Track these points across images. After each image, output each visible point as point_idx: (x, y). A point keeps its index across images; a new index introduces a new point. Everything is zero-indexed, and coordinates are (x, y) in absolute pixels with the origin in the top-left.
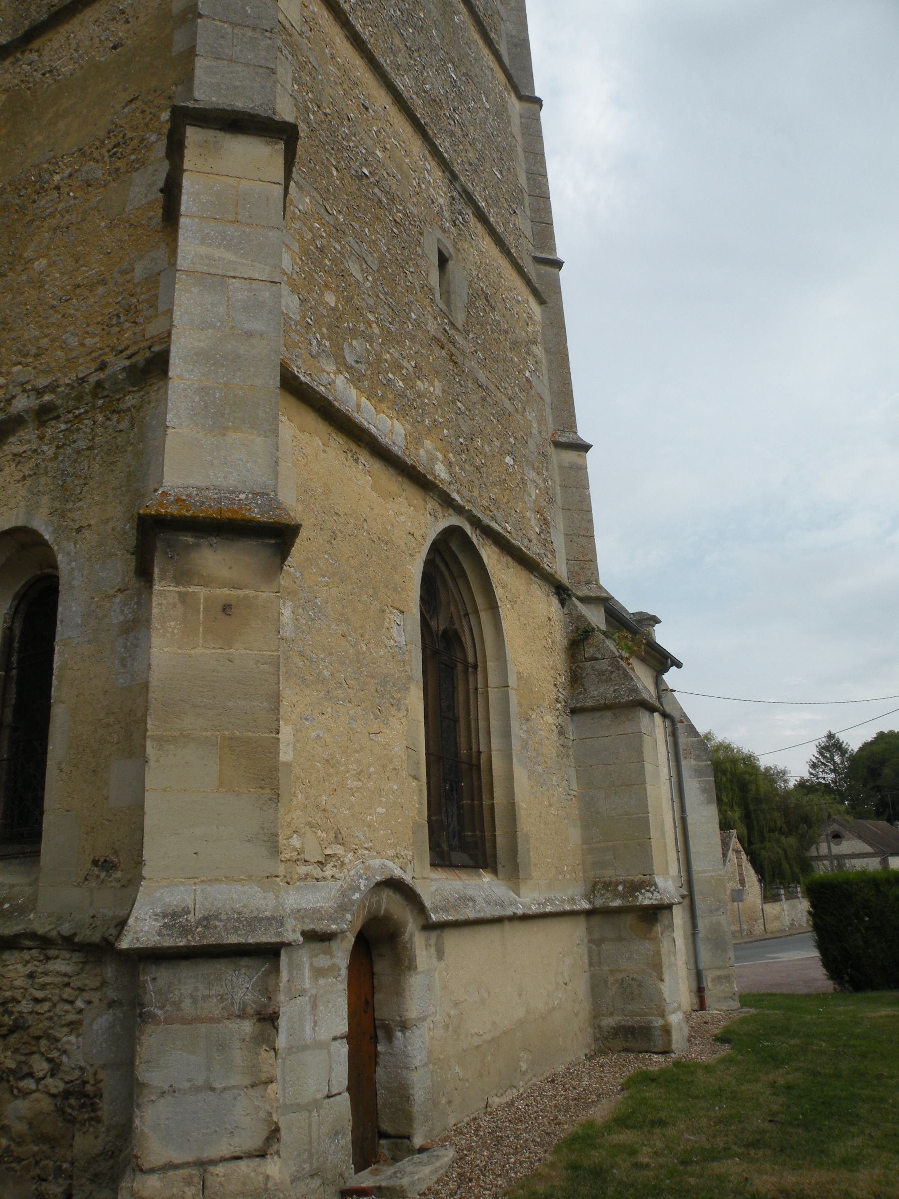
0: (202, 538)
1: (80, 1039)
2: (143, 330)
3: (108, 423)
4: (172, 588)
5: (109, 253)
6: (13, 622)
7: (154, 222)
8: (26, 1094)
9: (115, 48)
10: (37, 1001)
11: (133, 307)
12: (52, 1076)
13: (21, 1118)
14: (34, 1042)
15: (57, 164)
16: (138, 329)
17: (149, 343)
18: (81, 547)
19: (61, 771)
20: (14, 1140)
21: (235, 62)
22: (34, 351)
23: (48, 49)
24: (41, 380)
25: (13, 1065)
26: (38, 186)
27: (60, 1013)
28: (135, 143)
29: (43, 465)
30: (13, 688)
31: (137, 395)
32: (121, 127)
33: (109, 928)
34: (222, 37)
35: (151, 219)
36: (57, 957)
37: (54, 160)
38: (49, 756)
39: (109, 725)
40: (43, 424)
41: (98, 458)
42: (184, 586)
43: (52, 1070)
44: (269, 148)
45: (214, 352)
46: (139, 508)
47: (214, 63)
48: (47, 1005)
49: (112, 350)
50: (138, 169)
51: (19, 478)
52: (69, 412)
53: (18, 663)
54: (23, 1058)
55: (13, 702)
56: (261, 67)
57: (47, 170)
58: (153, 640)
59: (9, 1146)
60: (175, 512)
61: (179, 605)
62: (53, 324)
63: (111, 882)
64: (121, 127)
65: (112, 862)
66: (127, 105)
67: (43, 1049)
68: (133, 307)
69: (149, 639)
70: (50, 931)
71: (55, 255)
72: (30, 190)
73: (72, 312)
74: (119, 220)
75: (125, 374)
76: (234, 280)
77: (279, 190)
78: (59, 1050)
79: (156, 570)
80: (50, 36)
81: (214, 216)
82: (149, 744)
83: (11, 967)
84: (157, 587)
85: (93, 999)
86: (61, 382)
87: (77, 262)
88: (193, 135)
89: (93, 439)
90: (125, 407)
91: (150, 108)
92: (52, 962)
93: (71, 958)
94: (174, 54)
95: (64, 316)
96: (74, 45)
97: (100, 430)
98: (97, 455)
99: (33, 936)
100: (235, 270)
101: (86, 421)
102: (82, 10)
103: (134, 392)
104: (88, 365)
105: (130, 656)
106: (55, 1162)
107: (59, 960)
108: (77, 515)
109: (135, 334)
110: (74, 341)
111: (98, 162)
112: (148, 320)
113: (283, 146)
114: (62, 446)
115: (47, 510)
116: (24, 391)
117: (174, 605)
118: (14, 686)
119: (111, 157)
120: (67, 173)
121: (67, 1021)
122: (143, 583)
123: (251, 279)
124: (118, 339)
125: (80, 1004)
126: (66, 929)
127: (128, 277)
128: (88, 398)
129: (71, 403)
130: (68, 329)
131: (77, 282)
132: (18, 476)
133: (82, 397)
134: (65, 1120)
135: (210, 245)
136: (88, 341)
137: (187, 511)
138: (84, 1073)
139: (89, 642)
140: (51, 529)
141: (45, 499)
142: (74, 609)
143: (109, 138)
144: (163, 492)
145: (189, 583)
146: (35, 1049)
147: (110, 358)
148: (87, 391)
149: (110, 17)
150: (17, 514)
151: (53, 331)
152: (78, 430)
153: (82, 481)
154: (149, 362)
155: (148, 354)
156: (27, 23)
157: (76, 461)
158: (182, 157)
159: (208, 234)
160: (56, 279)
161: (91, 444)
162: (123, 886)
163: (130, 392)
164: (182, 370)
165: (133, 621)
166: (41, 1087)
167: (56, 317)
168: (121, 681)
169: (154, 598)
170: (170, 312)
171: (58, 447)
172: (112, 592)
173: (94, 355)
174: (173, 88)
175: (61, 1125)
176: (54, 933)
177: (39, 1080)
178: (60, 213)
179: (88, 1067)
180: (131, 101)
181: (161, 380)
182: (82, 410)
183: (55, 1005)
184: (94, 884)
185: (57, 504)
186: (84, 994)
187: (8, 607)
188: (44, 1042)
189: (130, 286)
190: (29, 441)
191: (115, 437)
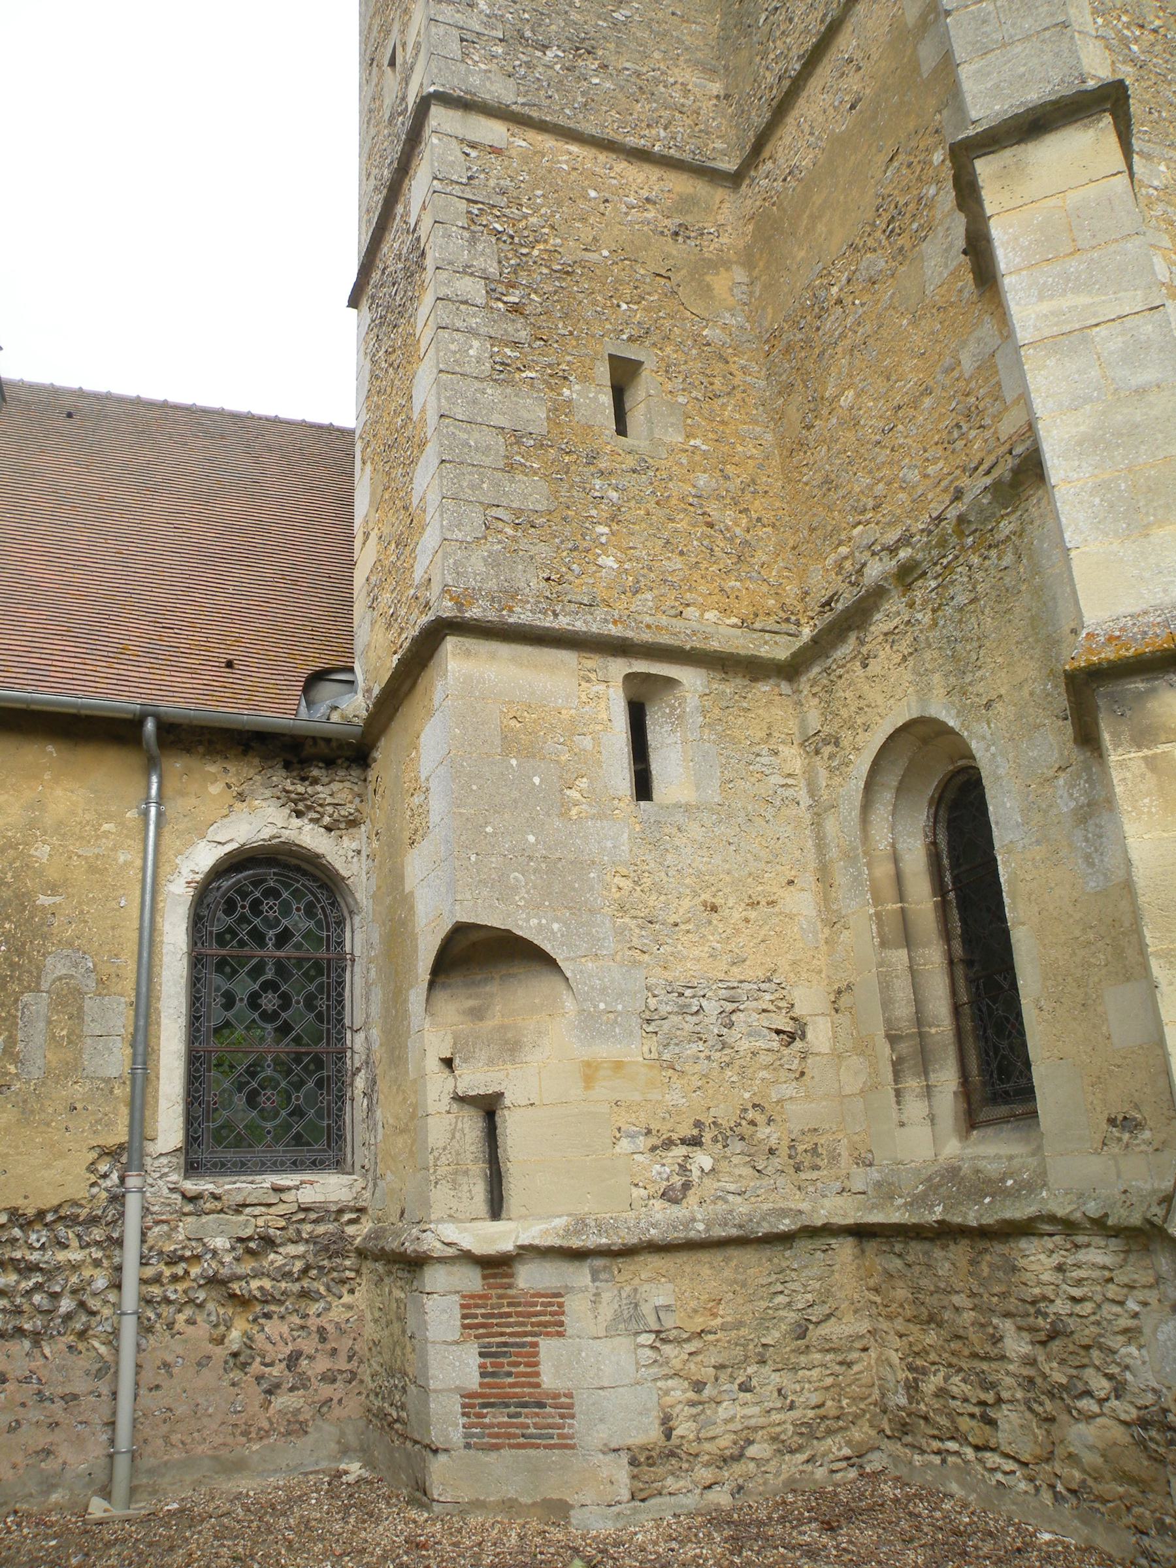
0: (1157, 679)
1: (1144, 1352)
2: (995, 432)
3: (987, 562)
4: (1133, 755)
5: (923, 354)
6: (935, 835)
7: (966, 294)
8: (1090, 1418)
9: (853, 107)
10: (1074, 1299)
11: (973, 408)
12: (1117, 1397)
13: (1091, 1448)
14: (1083, 1353)
15: (830, 273)
16: (988, 434)
17: (1007, 447)
18: (997, 727)
19: (1041, 1009)
20: (1089, 1475)
21: (1010, 44)
22: (871, 503)
23: (781, 149)
24: (889, 535)
25: (1064, 1381)
26: (816, 309)
27: (1109, 1317)
28: (912, 206)
29: (922, 638)
30: (955, 914)
31: (1013, 518)
32: (889, 196)
33: (1150, 1206)
34: (984, 22)
35: (960, 291)
36: (1088, 1245)
37: (825, 272)
38: (1022, 992)
39: (1089, 943)
40: (908, 587)
41: (987, 611)
42: (1149, 748)
43: (1116, 1390)
44: (1091, 132)
45: (1100, 432)
46: (1064, 664)
47: (983, 62)
48: (1088, 1307)
49: (964, 471)
50: (926, 236)
51: (898, 660)
52: (935, 564)
53: (954, 883)
54: (1074, 1372)
55: (959, 931)
56: (1045, 29)
57: (821, 286)
58: (1126, 827)
59: (1084, 1481)
60: (1112, 656)
61: (1149, 775)
62: (883, 463)
63: (1138, 1145)
64: (889, 196)
65: (1135, 1119)
66: (888, 168)
67: (1097, 1363)
68: (973, 408)
69: (1120, 826)
70: (1071, 1212)
71: (861, 380)
72: (809, 318)
73: (901, 441)
74: (922, 308)
75: (989, 496)
76: (1098, 329)
77: (1125, 177)
78: (1119, 1364)
79: (1106, 737)
80: (779, 134)
81: (1045, 258)
82: (1154, 963)
83: (1032, 1258)
84: (1113, 758)
85: (1150, 1300)
86: (913, 530)
87: (888, 380)
88: (984, 168)
89: (974, 588)
90: (1002, 536)
91: (916, 156)
92: (1083, 1251)
93: (1107, 1246)
94: (925, 76)
95: (892, 450)
96: (807, 129)
97: (979, 576)
98: (985, 606)
99: (1052, 1219)
100: (1095, 314)
101: (959, 569)
102: (805, 85)
103: (1007, 514)
104: (940, 499)
105: (1096, 850)
106: (1153, 1512)
107: (1092, 1249)
108: (980, 688)
109: (986, 441)
110: (914, 476)
111: (875, 250)
112: (997, 418)
113: (1110, 119)
114: (939, 608)
115: (942, 690)
116: (874, 554)
117: (1143, 776)
118: (955, 912)
119: (889, 237)
120: (844, 279)
121: (1121, 1328)
122: (1089, 754)
123: (1119, 317)
124: (967, 455)
125: (1132, 1305)
126: (1093, 1209)
127: (956, 374)
128: (954, 540)
129: (934, 552)
130: (903, 464)
131: (895, 403)
132: (897, 658)
133: (946, 541)
134: (1150, 1458)
135: (1052, 297)
136: (930, 470)
137: (1127, 650)
138: (1160, 1397)
139: (1038, 842)
140: (954, 712)
141: (937, 678)
142: (1008, 805)
143: (879, 216)
144: (1088, 634)
145: (1155, 742)
146: (1086, 1361)
147: (964, 481)
148: (950, 531)
149: (836, 74)
150: (908, 705)
151: (886, 471)
152: (952, 582)
153: (975, 644)
154: (1017, 471)
155: (1011, 462)
156: (751, 133)
157: (960, 621)
158: (979, 201)
159: (1045, 283)
160: (870, 409)
161: (973, 595)
162: (1157, 1150)
163: (1002, 516)
164: (1065, 471)
165: (1089, 805)
166: (1105, 1410)
167: (884, 455)
168: (1092, 884)
169: (1114, 773)
170: (1024, 399)
171: (934, 611)
172: (1051, 773)
173: (943, 484)
174: (938, 117)
175: (1146, 1463)
176: (1078, 1215)
177: (1101, 1401)
178: (850, 329)
179: (1164, 1390)
180: (891, 159)
181: (1038, 488)
182: (951, 557)
183: (1099, 1306)
184: (1115, 1149)
185: (952, 680)
186: (1136, 1292)
187: (925, 817)
188: (1095, 1353)
189: (962, 384)
190: (898, 613)
191: (1001, 578)
